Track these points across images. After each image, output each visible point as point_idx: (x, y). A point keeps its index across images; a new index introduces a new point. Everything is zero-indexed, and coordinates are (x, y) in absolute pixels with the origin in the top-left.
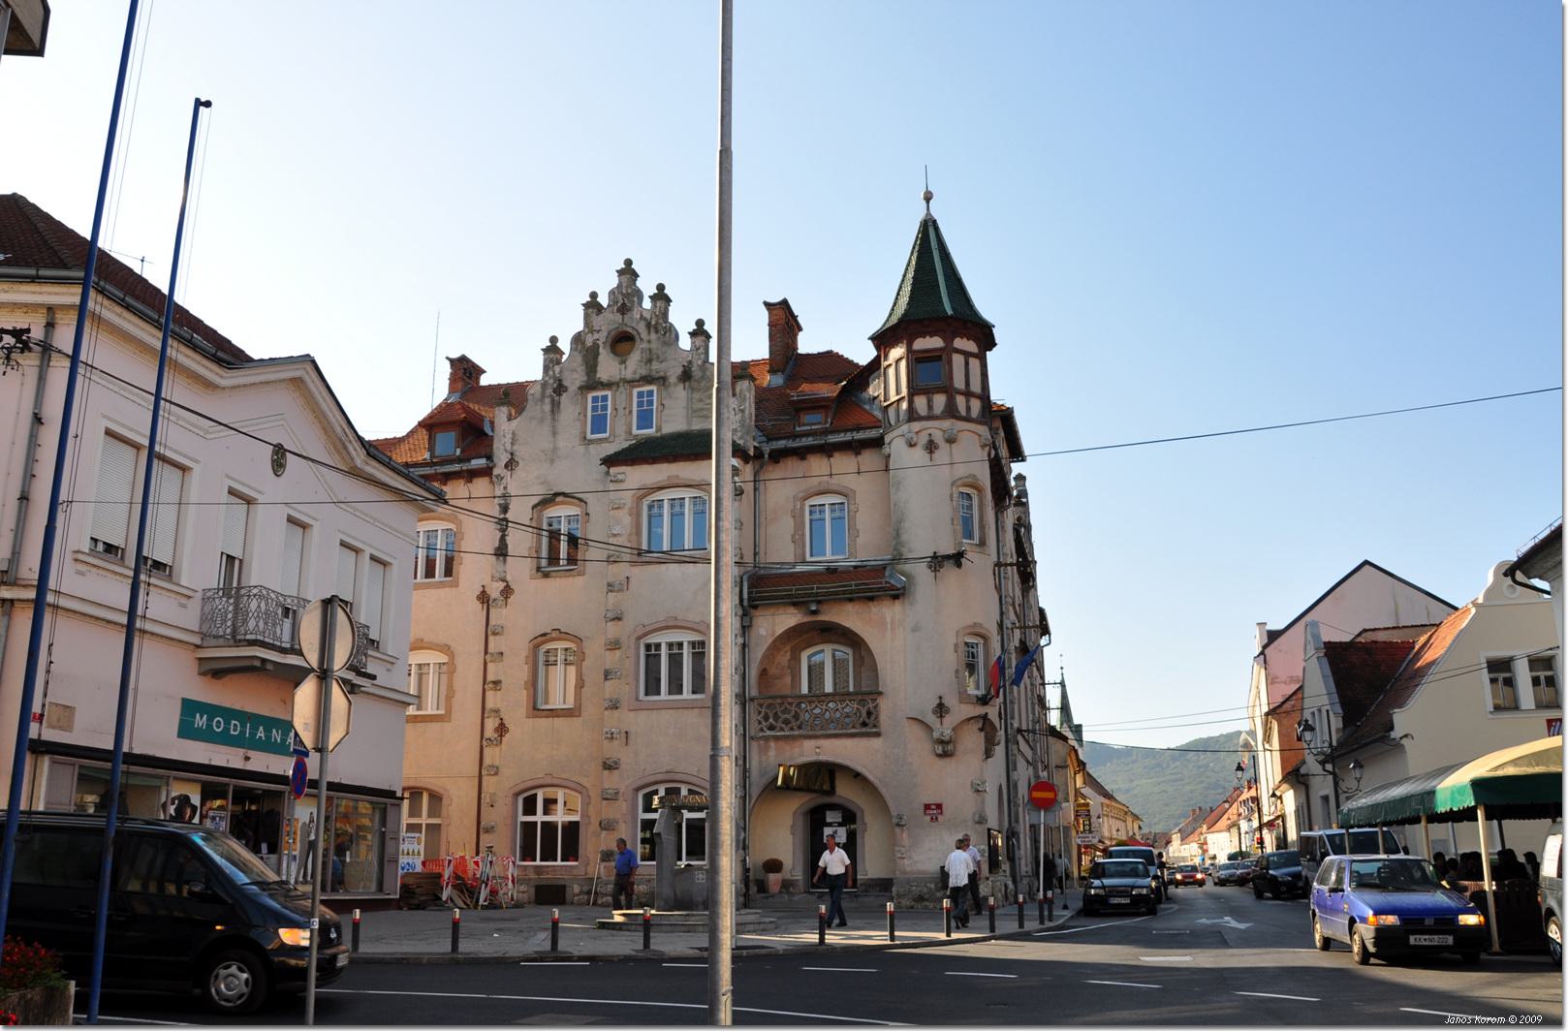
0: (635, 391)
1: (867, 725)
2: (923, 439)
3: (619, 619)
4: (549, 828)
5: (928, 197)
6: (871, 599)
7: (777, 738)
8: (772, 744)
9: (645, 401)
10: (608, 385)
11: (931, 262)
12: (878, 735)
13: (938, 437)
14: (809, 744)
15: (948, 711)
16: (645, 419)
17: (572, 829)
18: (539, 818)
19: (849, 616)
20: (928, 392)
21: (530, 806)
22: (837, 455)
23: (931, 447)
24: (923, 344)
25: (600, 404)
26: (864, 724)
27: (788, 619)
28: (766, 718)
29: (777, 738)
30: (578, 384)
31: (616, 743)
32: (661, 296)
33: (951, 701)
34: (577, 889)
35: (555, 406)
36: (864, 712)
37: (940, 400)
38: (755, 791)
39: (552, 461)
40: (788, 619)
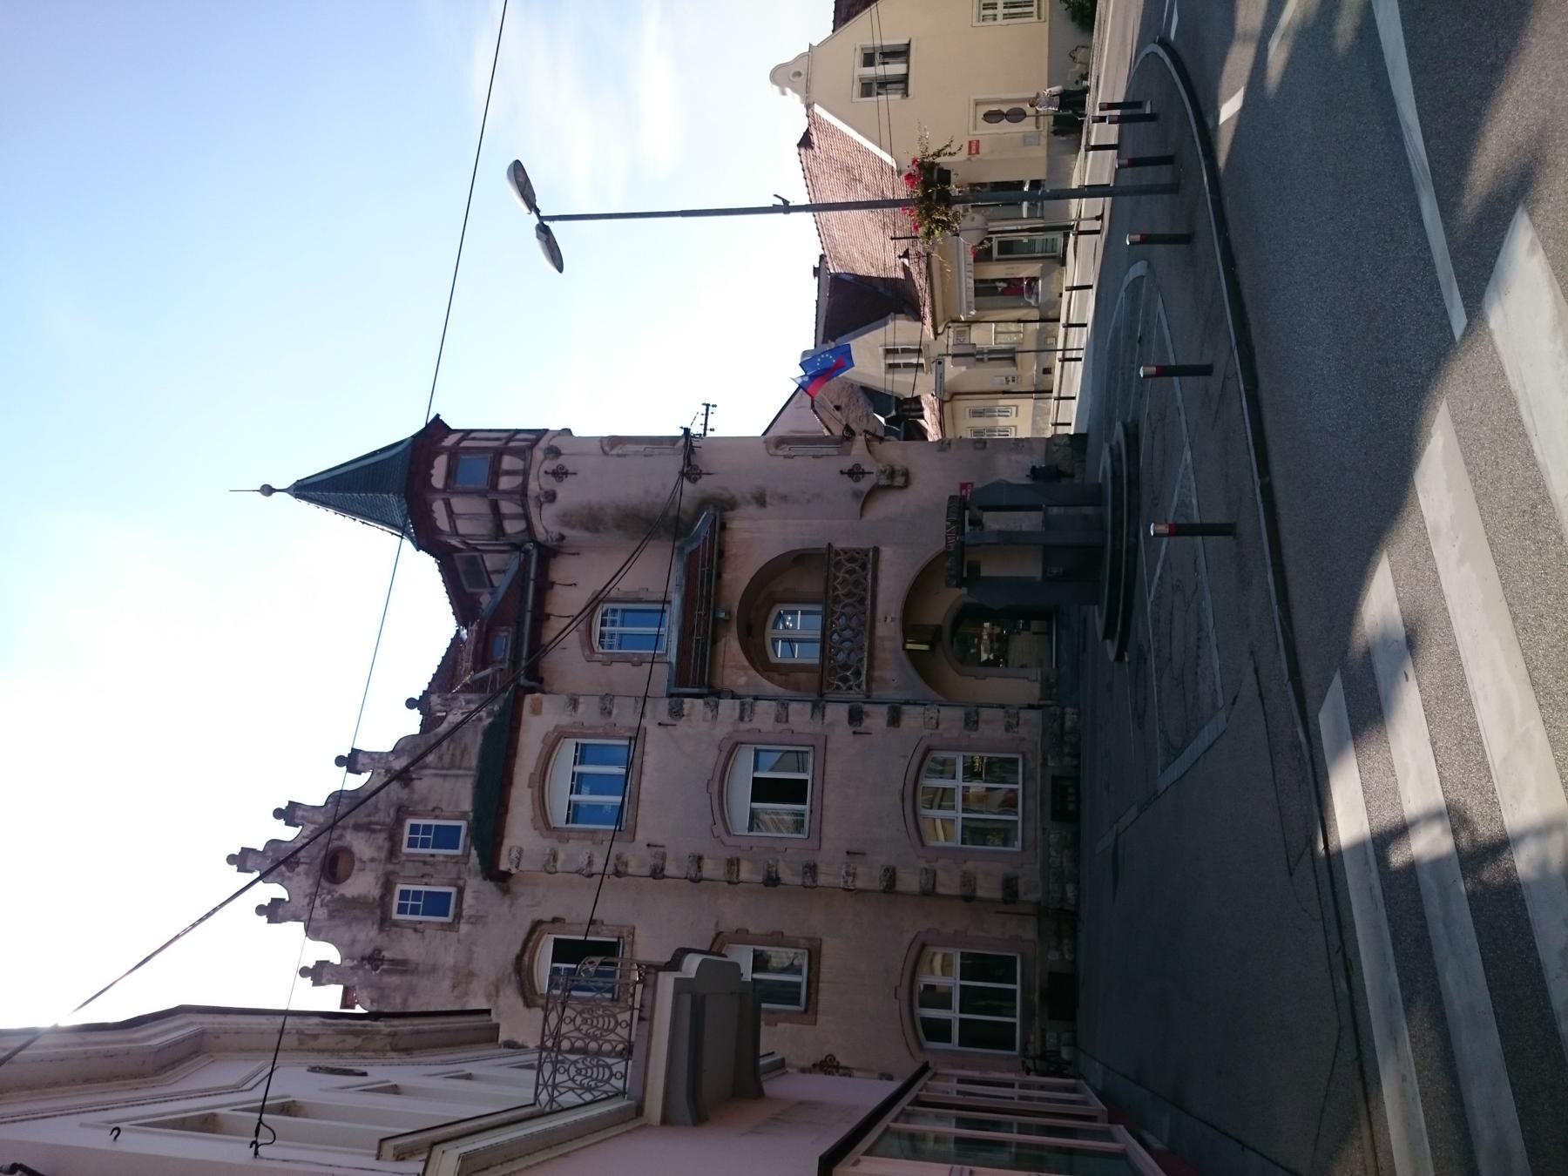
0: (405, 849)
1: (865, 562)
2: (549, 483)
3: (700, 858)
4: (970, 999)
5: (268, 490)
6: (721, 554)
7: (871, 667)
8: (877, 673)
9: (423, 836)
10: (387, 886)
11: (346, 489)
12: (876, 550)
13: (550, 465)
14: (882, 630)
15: (831, 1057)
16: (446, 837)
17: (975, 966)
18: (954, 1015)
19: (738, 578)
20: (496, 473)
21: (938, 1030)
22: (548, 610)
23: (560, 474)
24: (438, 478)
25: (414, 902)
26: (863, 567)
27: (731, 646)
28: (845, 680)
29: (871, 667)
30: (373, 932)
31: (860, 870)
32: (289, 814)
33: (847, 463)
34: (1053, 956)
35: (401, 966)
36: (849, 566)
37: (508, 462)
38: (933, 694)
39: (471, 974)
40: (731, 646)
